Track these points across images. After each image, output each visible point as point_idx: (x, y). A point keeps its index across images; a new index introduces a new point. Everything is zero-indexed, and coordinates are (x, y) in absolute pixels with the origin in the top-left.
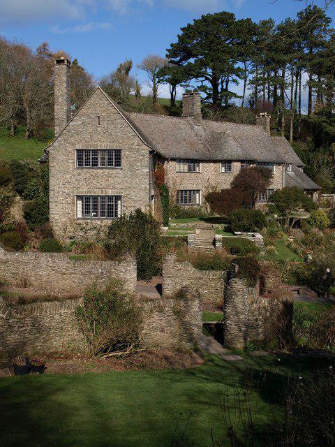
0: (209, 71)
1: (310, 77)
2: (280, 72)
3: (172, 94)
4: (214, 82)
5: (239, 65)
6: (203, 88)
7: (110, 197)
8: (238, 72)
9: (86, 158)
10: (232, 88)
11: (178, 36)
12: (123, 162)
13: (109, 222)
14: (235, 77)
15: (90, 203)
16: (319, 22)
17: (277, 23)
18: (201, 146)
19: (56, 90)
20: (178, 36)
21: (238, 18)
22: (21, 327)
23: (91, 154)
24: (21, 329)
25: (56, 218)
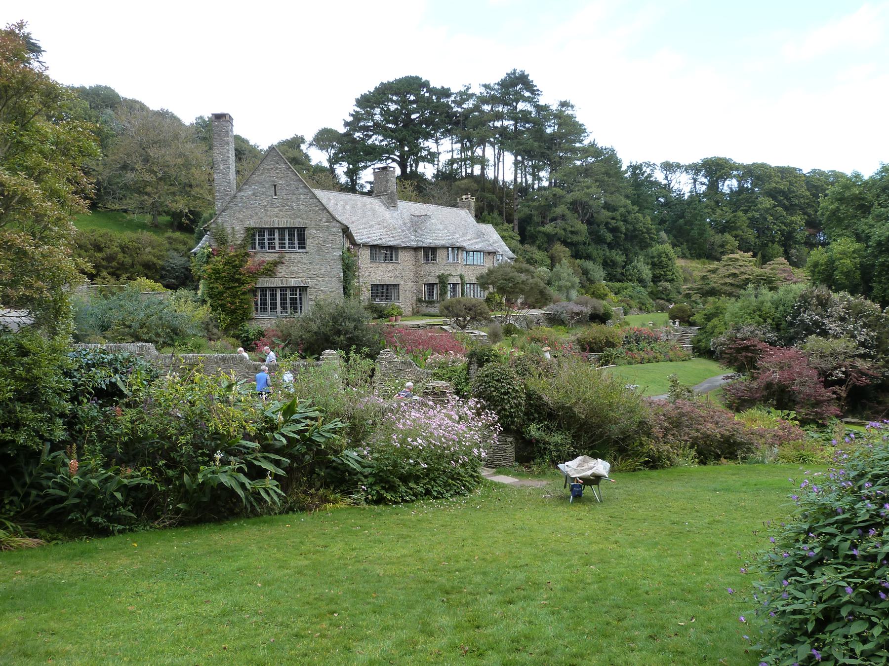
7: (293, 289)
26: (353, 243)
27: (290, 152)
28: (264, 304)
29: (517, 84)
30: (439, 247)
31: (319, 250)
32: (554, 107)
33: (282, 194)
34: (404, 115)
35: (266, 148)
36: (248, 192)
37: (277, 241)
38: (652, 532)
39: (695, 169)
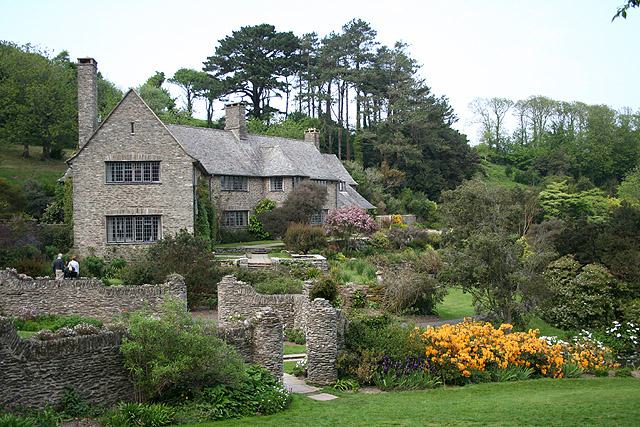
0: (250, 84)
1: (358, 93)
2: (326, 87)
3: (208, 111)
4: (256, 98)
5: (281, 79)
6: (243, 104)
7: (147, 217)
8: (283, 86)
9: (120, 171)
10: (275, 103)
11: (65, 54)
12: (162, 175)
13: (145, 246)
14: (277, 91)
15: (121, 224)
16: (366, 34)
17: (320, 37)
18: (248, 163)
19: (79, 95)
20: (65, 54)
21: (278, 30)
22: (44, 372)
23: (124, 166)
24: (44, 376)
25: (83, 243)
26: (205, 173)
27: (153, 92)
28: (129, 231)
29: (359, 30)
30: (285, 177)
31: (172, 179)
32: (391, 47)
33: (138, 131)
34: (255, 57)
35: (125, 90)
36: (107, 129)
37: (133, 174)
38: (14, 219)
39: (523, 105)
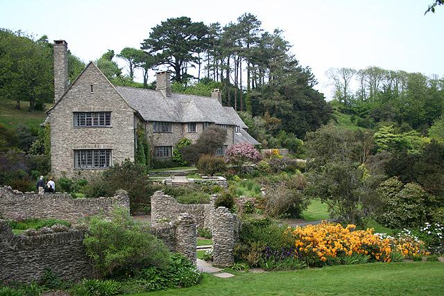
0: (174, 59)
1: (249, 65)
2: (226, 60)
3: (145, 77)
4: (177, 68)
5: (195, 55)
6: (169, 72)
7: (102, 151)
8: (196, 60)
9: (83, 119)
10: (190, 71)
12: (112, 122)
13: (101, 171)
14: (192, 63)
15: (84, 156)
16: (254, 24)
17: (222, 26)
18: (172, 113)
19: (55, 66)
21: (193, 21)
22: (31, 258)
23: (86, 115)
24: (30, 261)
25: (57, 168)
26: (142, 120)
27: (106, 64)
28: (90, 160)
29: (249, 21)
30: (198, 123)
31: (119, 124)
32: (271, 33)
33: (96, 91)
34: (177, 39)
35: (87, 63)
36: (74, 90)
37: (93, 120)
38: (10, 152)
39: (363, 73)
